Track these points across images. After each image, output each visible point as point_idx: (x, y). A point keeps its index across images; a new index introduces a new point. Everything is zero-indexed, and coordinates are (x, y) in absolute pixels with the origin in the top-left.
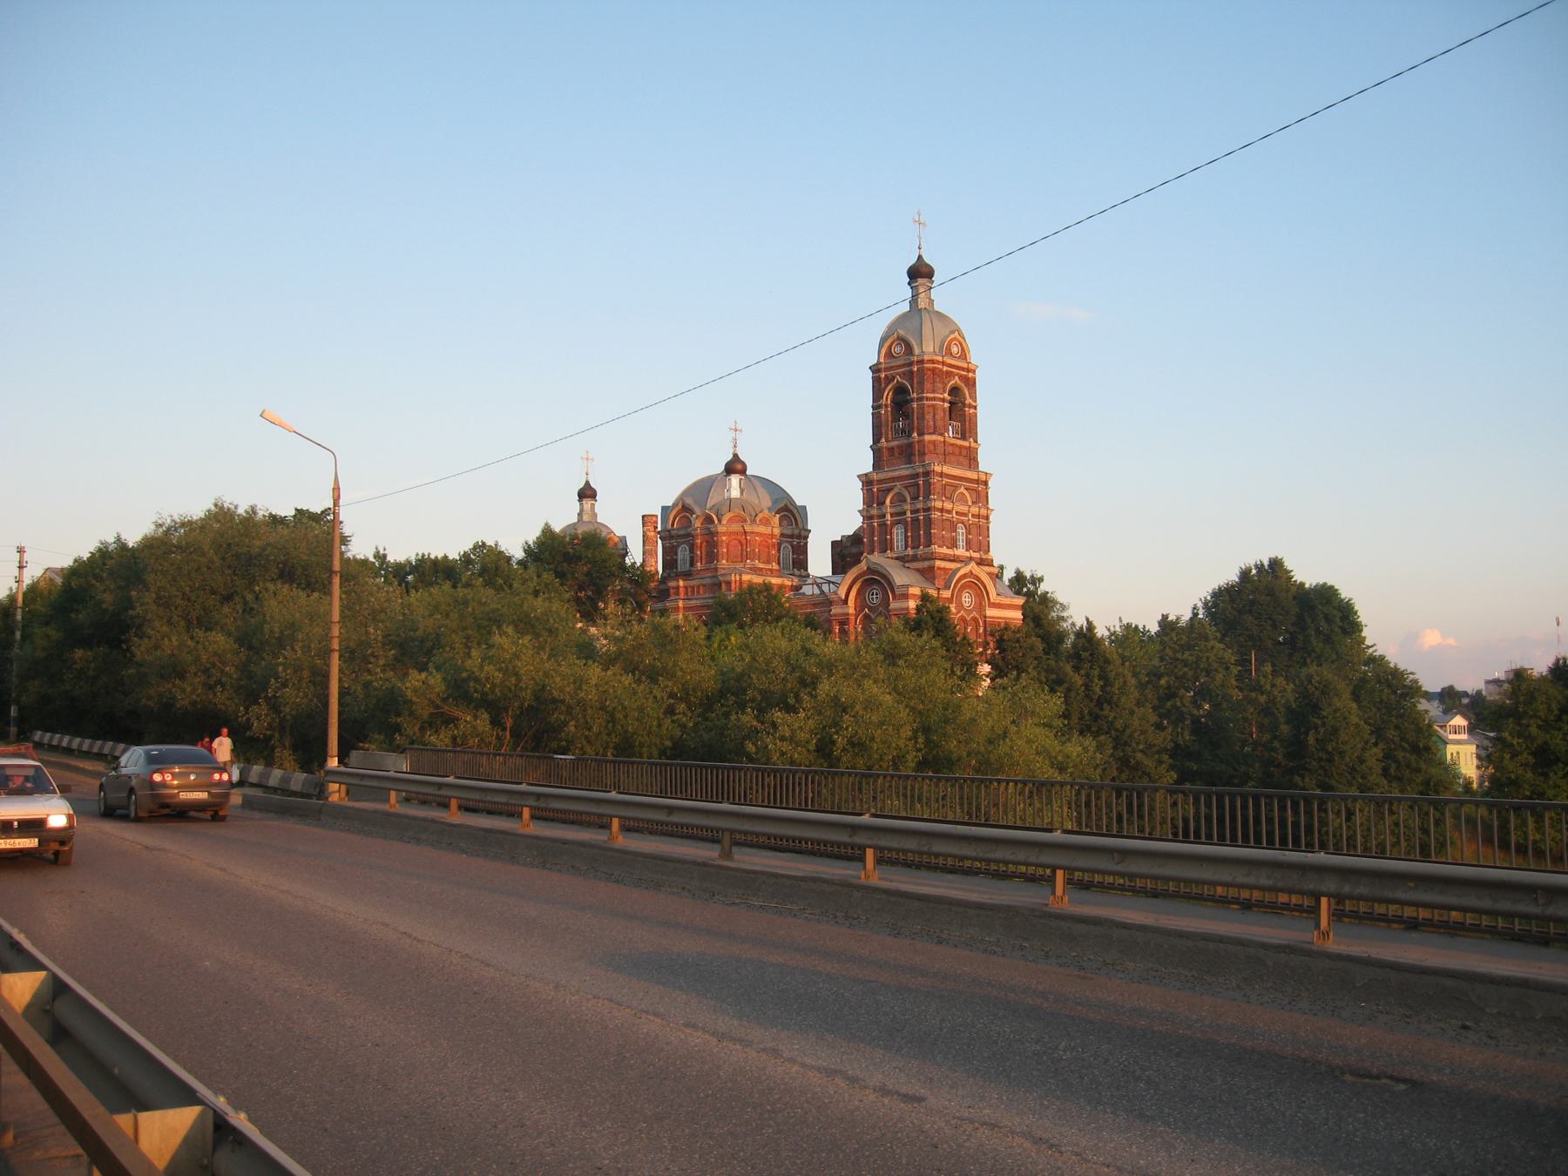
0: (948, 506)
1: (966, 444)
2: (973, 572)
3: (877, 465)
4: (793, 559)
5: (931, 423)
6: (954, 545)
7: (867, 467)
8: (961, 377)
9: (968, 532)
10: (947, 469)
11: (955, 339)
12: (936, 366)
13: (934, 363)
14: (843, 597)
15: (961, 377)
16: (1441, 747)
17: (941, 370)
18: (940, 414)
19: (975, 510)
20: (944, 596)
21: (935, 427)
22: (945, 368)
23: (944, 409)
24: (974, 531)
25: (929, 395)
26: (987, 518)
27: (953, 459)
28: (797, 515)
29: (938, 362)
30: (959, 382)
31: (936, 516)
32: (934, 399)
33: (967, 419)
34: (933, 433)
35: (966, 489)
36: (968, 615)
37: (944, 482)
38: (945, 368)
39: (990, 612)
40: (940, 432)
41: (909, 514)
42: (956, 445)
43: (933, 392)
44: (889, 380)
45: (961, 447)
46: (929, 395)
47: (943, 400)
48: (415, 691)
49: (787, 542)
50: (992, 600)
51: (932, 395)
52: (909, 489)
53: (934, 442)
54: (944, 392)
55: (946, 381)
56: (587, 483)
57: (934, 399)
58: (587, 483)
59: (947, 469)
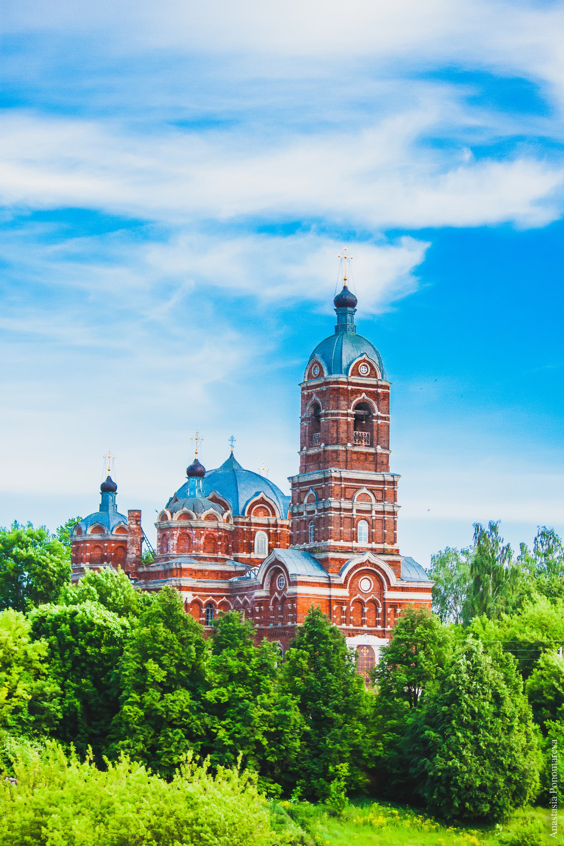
0: (346, 504)
1: (372, 450)
2: (371, 561)
3: (304, 469)
4: (269, 545)
5: (335, 435)
6: (354, 537)
7: (295, 471)
8: (368, 393)
9: (371, 526)
10: (345, 474)
11: (364, 361)
12: (341, 386)
13: (339, 384)
14: (261, 583)
15: (318, 393)
16: (417, 811)
17: (347, 390)
18: (343, 427)
19: (379, 507)
20: (335, 582)
21: (338, 438)
22: (350, 388)
23: (348, 423)
24: (379, 525)
25: (333, 411)
26: (394, 513)
27: (356, 464)
28: (274, 507)
29: (343, 383)
30: (366, 398)
31: (333, 515)
32: (337, 414)
33: (375, 428)
34: (337, 444)
35: (371, 490)
36: (366, 598)
37: (343, 486)
38: (350, 388)
39: (389, 595)
40: (343, 442)
41: (305, 514)
42: (361, 453)
43: (338, 408)
44: (309, 396)
45: (366, 454)
46: (333, 411)
47: (347, 415)
48: (159, 622)
49: (262, 530)
50: (392, 585)
51: (336, 411)
52: (373, 491)
53: (336, 452)
54: (349, 408)
55: (352, 398)
56: (109, 478)
57: (337, 414)
58: (109, 478)
59: (345, 474)
